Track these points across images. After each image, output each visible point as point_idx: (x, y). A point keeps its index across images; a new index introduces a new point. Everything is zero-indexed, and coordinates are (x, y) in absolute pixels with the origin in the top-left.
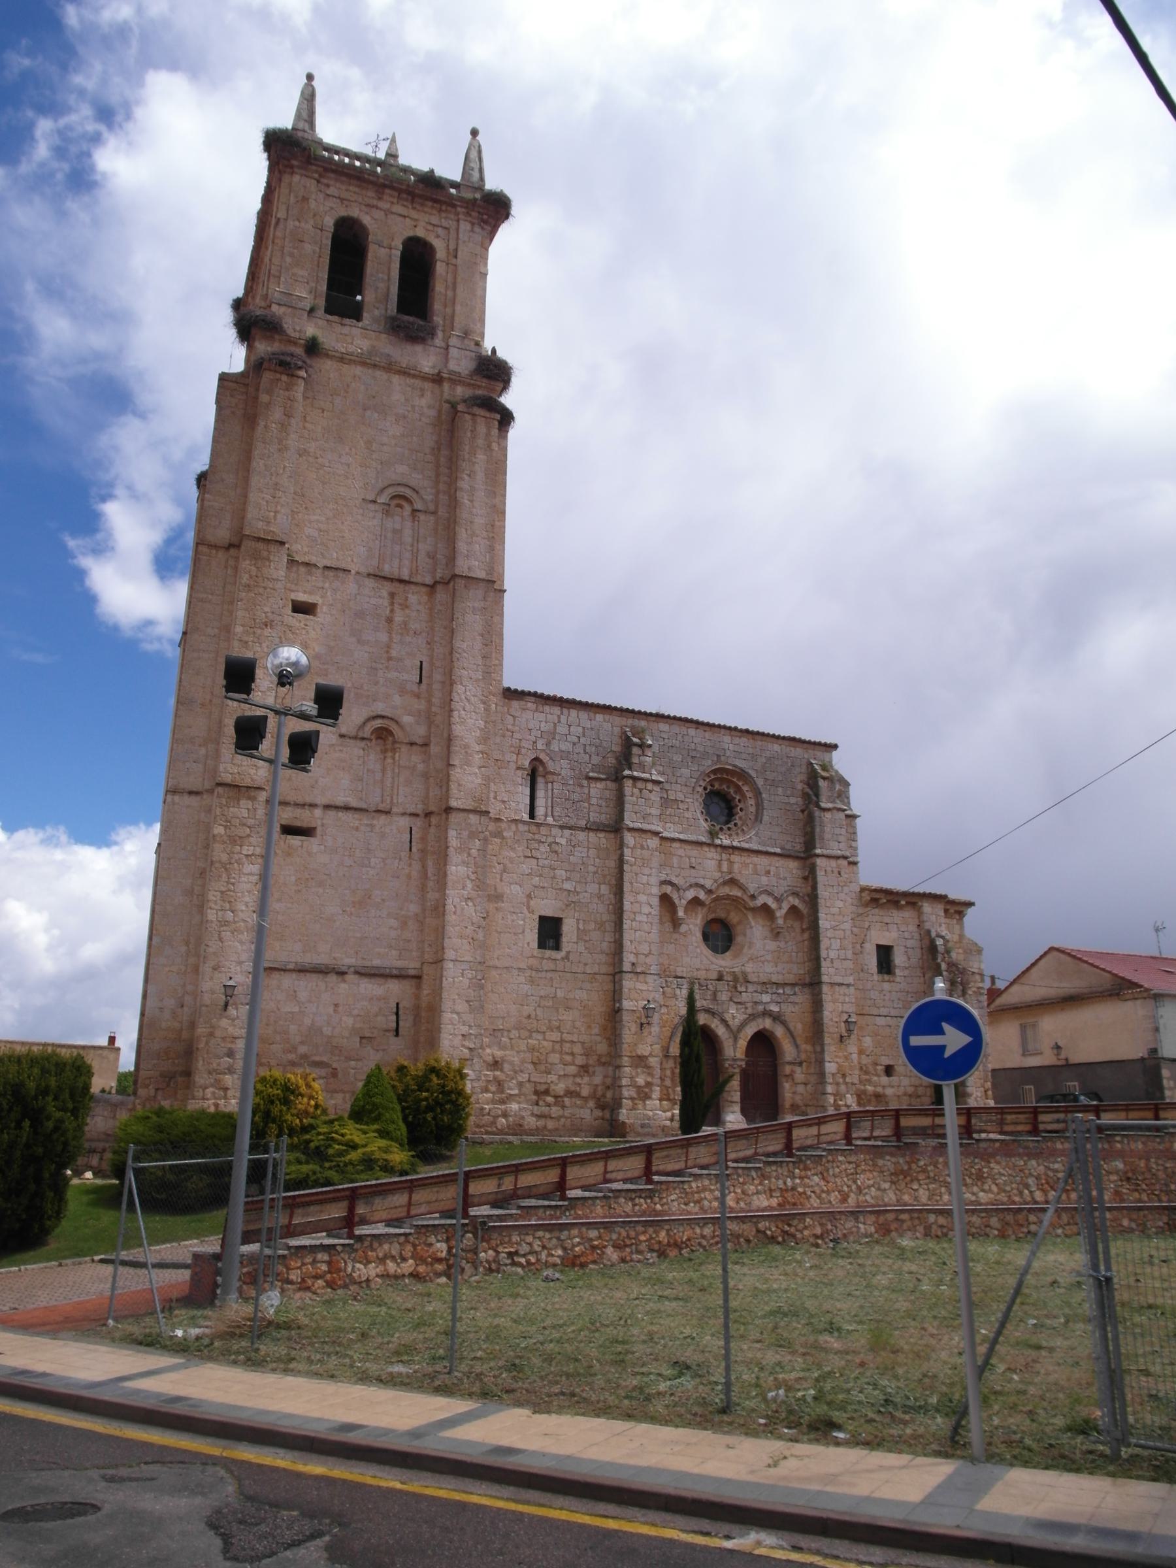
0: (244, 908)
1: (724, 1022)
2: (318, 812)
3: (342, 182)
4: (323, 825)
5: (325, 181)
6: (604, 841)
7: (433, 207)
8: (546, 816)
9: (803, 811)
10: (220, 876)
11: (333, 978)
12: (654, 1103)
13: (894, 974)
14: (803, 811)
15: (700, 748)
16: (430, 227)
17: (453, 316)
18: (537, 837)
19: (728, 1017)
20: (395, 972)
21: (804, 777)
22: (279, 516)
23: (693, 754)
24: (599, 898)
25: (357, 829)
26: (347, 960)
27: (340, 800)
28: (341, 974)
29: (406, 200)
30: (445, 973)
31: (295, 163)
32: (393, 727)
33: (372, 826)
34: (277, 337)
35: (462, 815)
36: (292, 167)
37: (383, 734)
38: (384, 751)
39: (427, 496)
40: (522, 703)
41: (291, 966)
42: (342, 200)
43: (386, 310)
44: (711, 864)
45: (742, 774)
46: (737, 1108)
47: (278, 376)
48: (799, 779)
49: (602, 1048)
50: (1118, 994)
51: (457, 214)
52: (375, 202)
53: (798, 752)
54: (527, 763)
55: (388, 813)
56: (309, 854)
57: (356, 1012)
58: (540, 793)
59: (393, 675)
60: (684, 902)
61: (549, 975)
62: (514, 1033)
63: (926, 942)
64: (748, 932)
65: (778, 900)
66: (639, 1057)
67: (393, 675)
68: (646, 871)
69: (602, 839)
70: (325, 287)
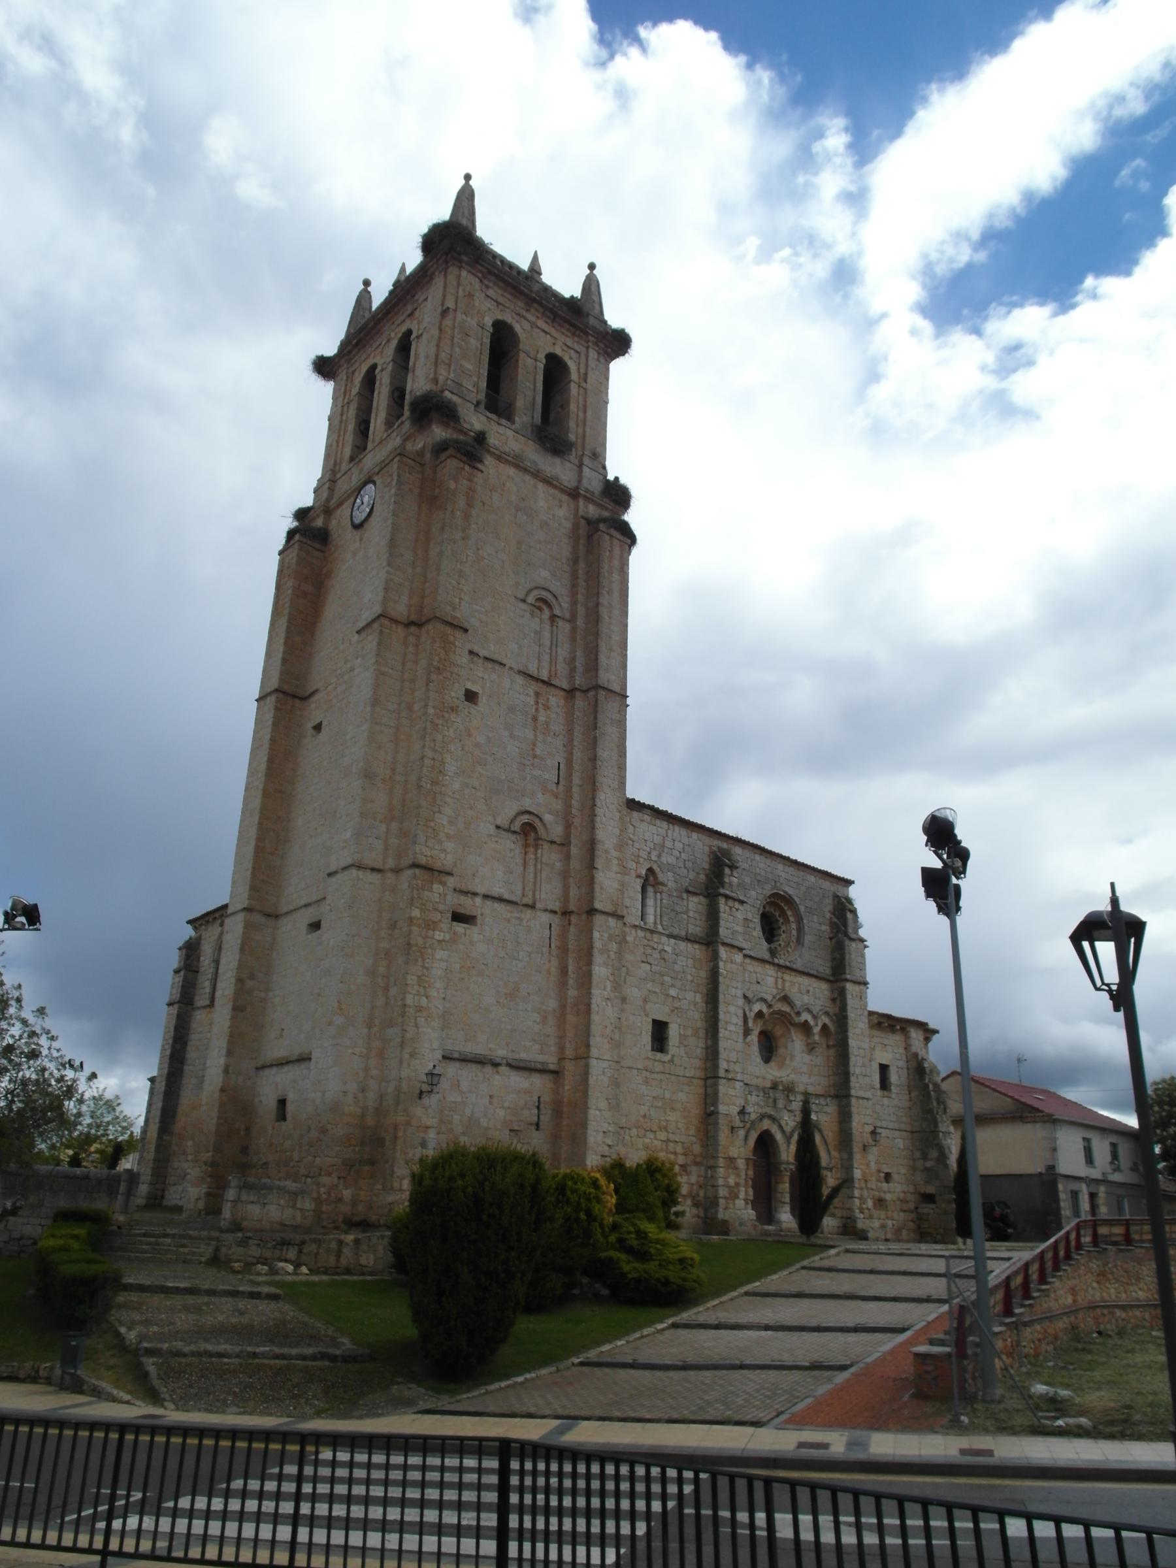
0: (435, 994)
1: (780, 1127)
2: (478, 901)
3: (499, 287)
4: (482, 915)
5: (486, 282)
6: (698, 952)
7: (568, 330)
8: (655, 923)
9: (831, 939)
10: (417, 960)
11: (489, 1069)
12: (740, 1203)
13: (890, 1090)
14: (831, 939)
15: (763, 873)
16: (565, 348)
17: (584, 436)
18: (651, 943)
19: (783, 1123)
20: (539, 1066)
21: (830, 908)
22: (463, 603)
23: (758, 878)
24: (695, 1005)
25: (508, 921)
26: (501, 1053)
27: (497, 890)
28: (496, 1065)
29: (549, 318)
30: (591, 1071)
31: (465, 258)
32: (537, 823)
33: (520, 919)
34: (452, 424)
35: (603, 917)
36: (461, 261)
37: (528, 830)
38: (526, 846)
39: (565, 602)
40: (641, 814)
41: (456, 1055)
42: (498, 303)
43: (533, 417)
44: (770, 981)
45: (789, 900)
46: (787, 1208)
47: (461, 465)
48: (828, 906)
49: (697, 1148)
50: (1021, 1117)
51: (587, 342)
52: (524, 313)
53: (826, 884)
54: (644, 872)
55: (532, 907)
56: (471, 943)
57: (506, 1104)
58: (650, 902)
59: (537, 772)
60: (753, 1014)
61: (660, 1076)
62: (634, 1132)
63: (913, 1064)
64: (790, 1045)
65: (815, 1017)
66: (730, 1158)
67: (537, 772)
68: (734, 984)
69: (696, 950)
70: (485, 385)
